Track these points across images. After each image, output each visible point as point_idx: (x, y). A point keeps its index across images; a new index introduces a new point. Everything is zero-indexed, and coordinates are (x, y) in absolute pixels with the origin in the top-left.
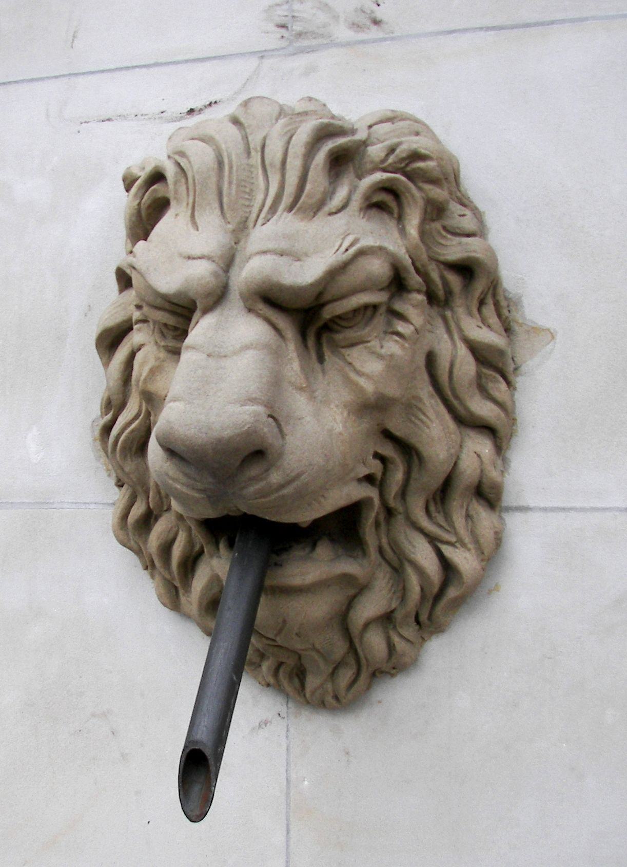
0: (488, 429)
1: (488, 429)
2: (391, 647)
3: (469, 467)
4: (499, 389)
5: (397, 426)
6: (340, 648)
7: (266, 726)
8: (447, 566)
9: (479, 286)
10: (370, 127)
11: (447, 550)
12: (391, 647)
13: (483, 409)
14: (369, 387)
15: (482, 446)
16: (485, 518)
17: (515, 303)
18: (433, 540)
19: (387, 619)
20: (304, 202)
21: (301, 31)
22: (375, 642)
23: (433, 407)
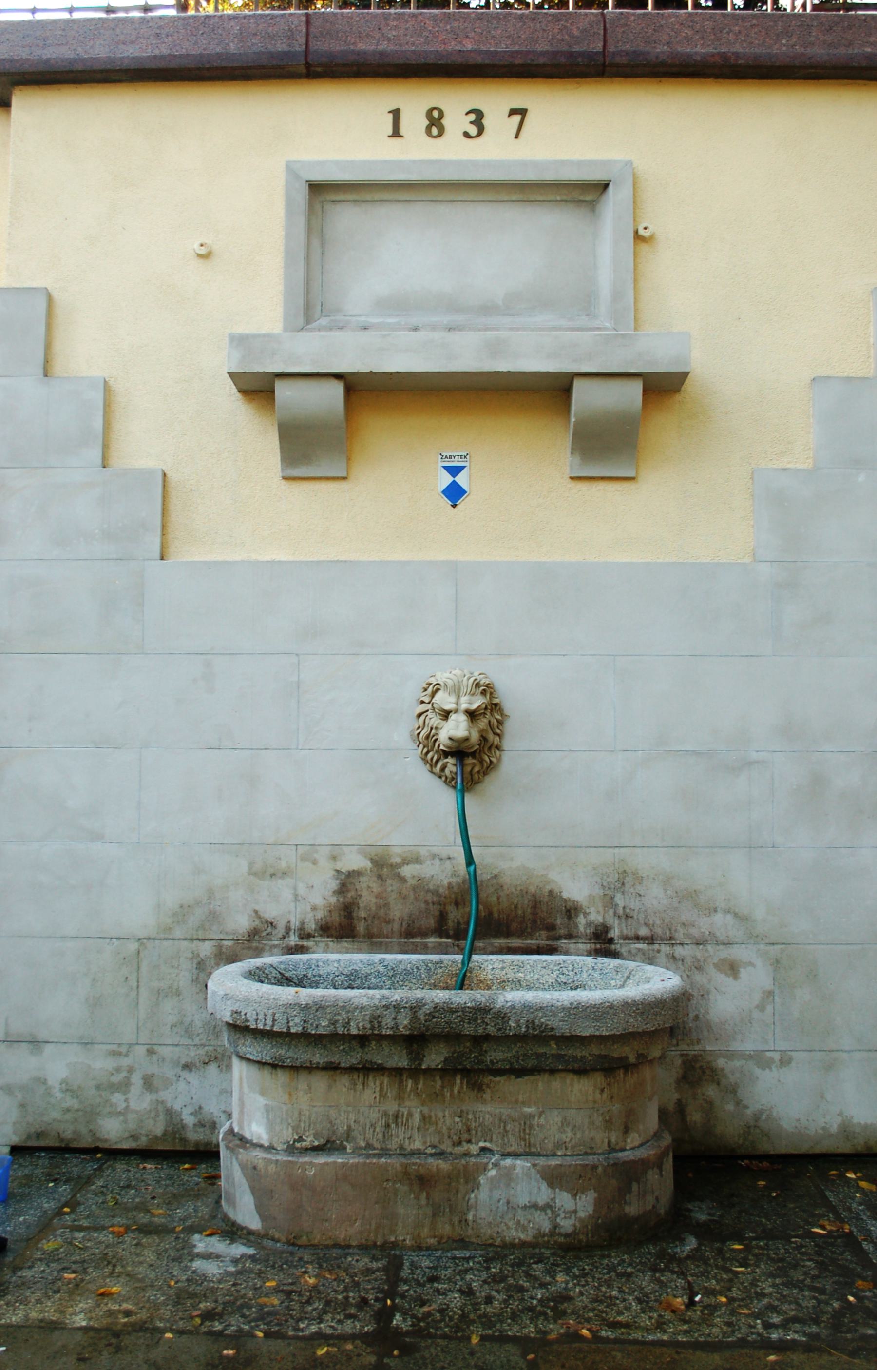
0: (498, 735)
1: (498, 735)
2: (479, 778)
3: (496, 743)
4: (501, 727)
5: (484, 735)
6: (469, 778)
7: (433, 876)
8: (490, 760)
9: (498, 708)
10: (344, 478)
11: (491, 758)
12: (479, 778)
13: (498, 731)
14: (481, 727)
15: (497, 738)
16: (498, 752)
17: (503, 710)
18: (488, 756)
19: (479, 772)
20: (575, 410)
21: (581, 906)
22: (476, 776)
23: (490, 731)
